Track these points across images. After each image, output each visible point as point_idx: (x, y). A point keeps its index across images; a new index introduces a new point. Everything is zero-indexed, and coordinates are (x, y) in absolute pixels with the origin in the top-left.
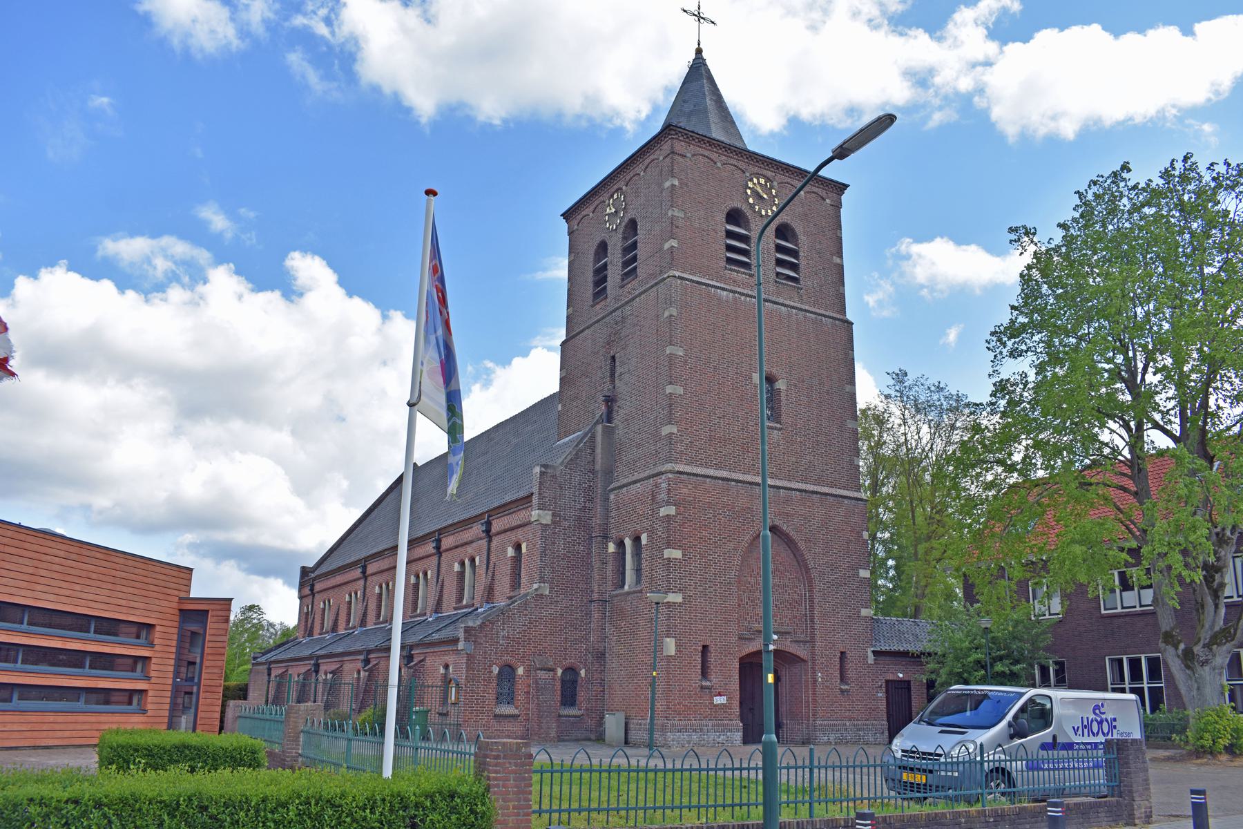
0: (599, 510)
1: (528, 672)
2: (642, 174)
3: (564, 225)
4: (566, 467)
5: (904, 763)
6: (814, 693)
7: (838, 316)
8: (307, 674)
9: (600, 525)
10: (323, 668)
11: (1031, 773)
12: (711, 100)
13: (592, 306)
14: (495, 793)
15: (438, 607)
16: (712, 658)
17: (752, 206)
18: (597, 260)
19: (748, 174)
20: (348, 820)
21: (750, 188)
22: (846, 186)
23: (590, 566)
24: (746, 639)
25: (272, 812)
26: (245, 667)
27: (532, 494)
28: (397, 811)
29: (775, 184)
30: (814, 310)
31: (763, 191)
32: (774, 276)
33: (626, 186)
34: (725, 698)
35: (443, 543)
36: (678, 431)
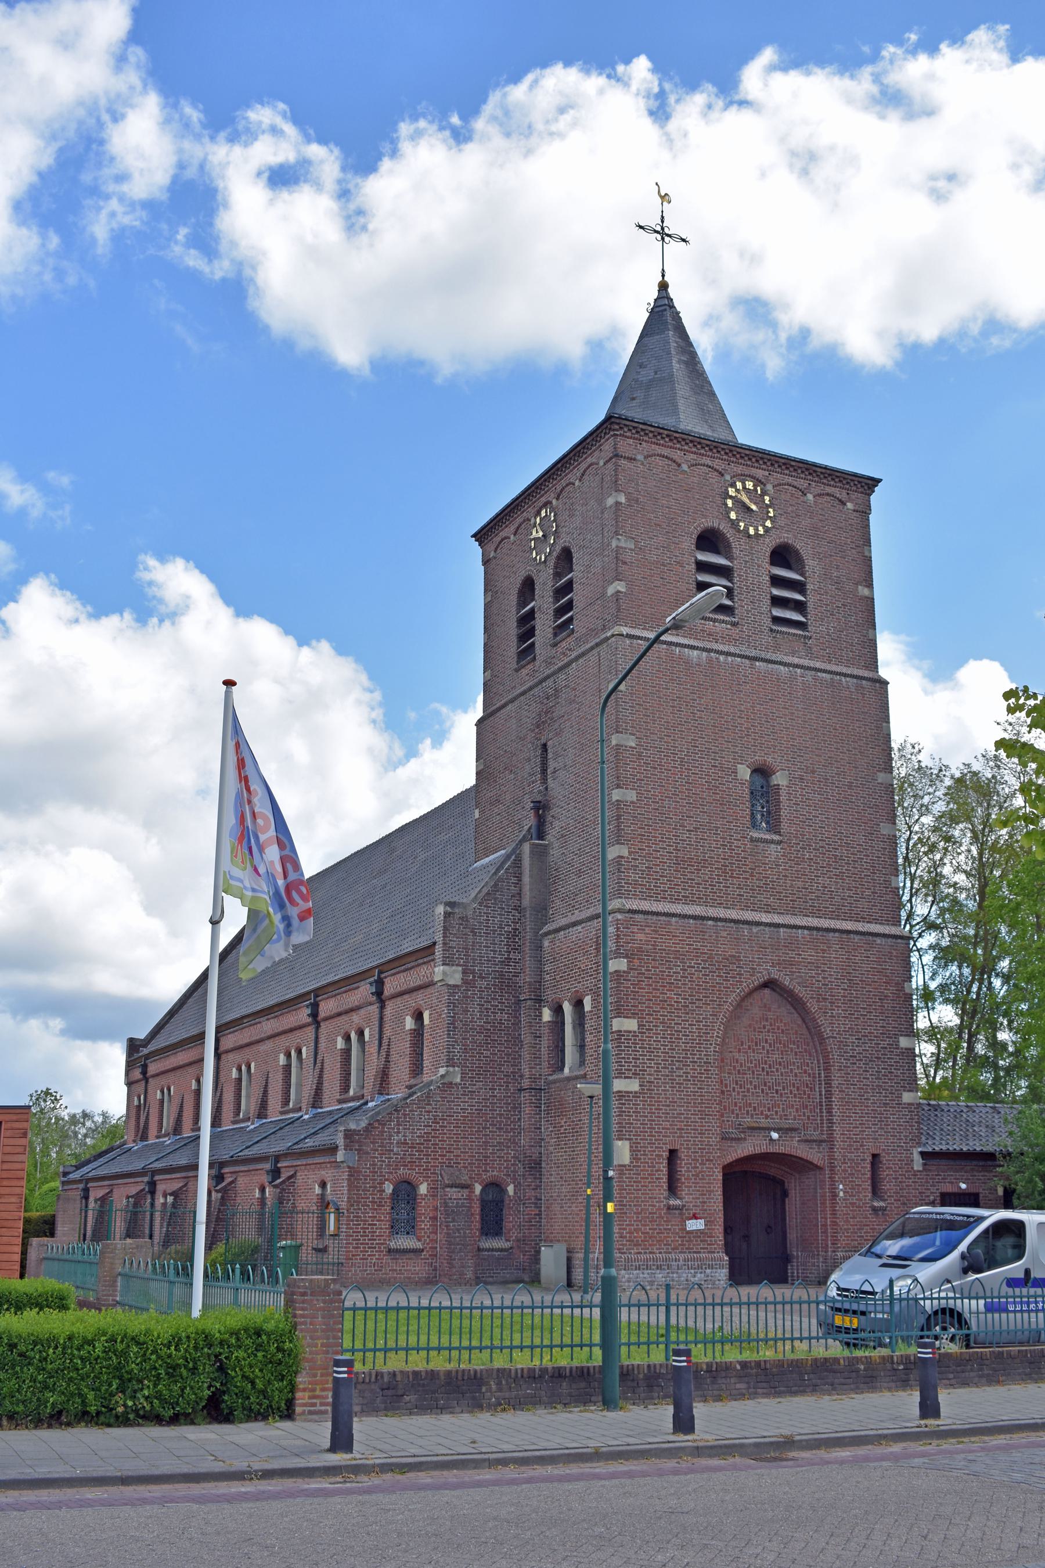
0: (528, 963)
1: (433, 1190)
2: (577, 483)
3: (476, 551)
4: (480, 904)
5: (838, 1305)
6: (834, 1213)
7: (866, 674)
8: (138, 1197)
9: (530, 984)
10: (160, 1188)
11: (989, 1316)
12: (679, 362)
13: (517, 670)
14: (302, 1330)
15: (317, 1100)
16: (683, 1168)
17: (734, 524)
18: (523, 604)
19: (728, 477)
20: (154, 1357)
21: (731, 497)
22: (878, 481)
23: (518, 1041)
24: (732, 1139)
25: (79, 1350)
26: (53, 1184)
27: (434, 944)
28: (202, 1348)
29: (769, 487)
30: (828, 667)
31: (751, 500)
32: (768, 622)
33: (557, 499)
34: (702, 1221)
35: (321, 1008)
36: (630, 853)
